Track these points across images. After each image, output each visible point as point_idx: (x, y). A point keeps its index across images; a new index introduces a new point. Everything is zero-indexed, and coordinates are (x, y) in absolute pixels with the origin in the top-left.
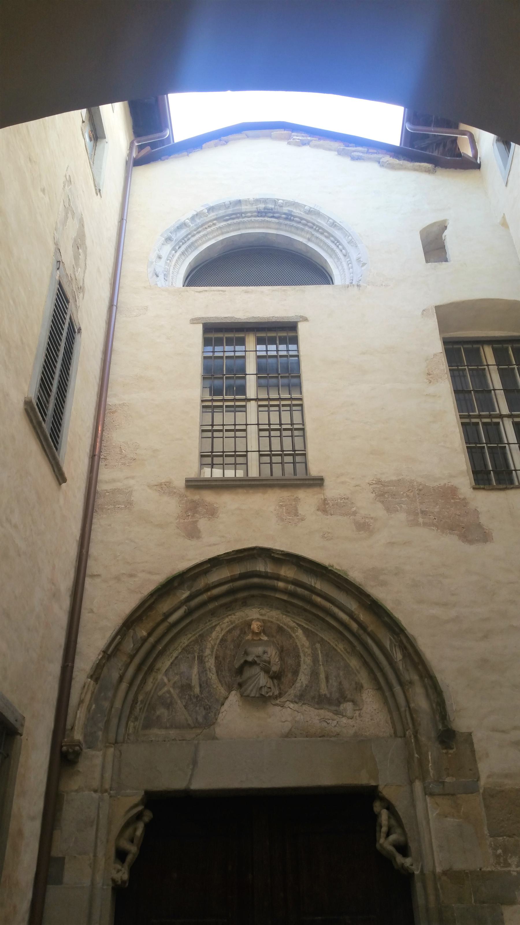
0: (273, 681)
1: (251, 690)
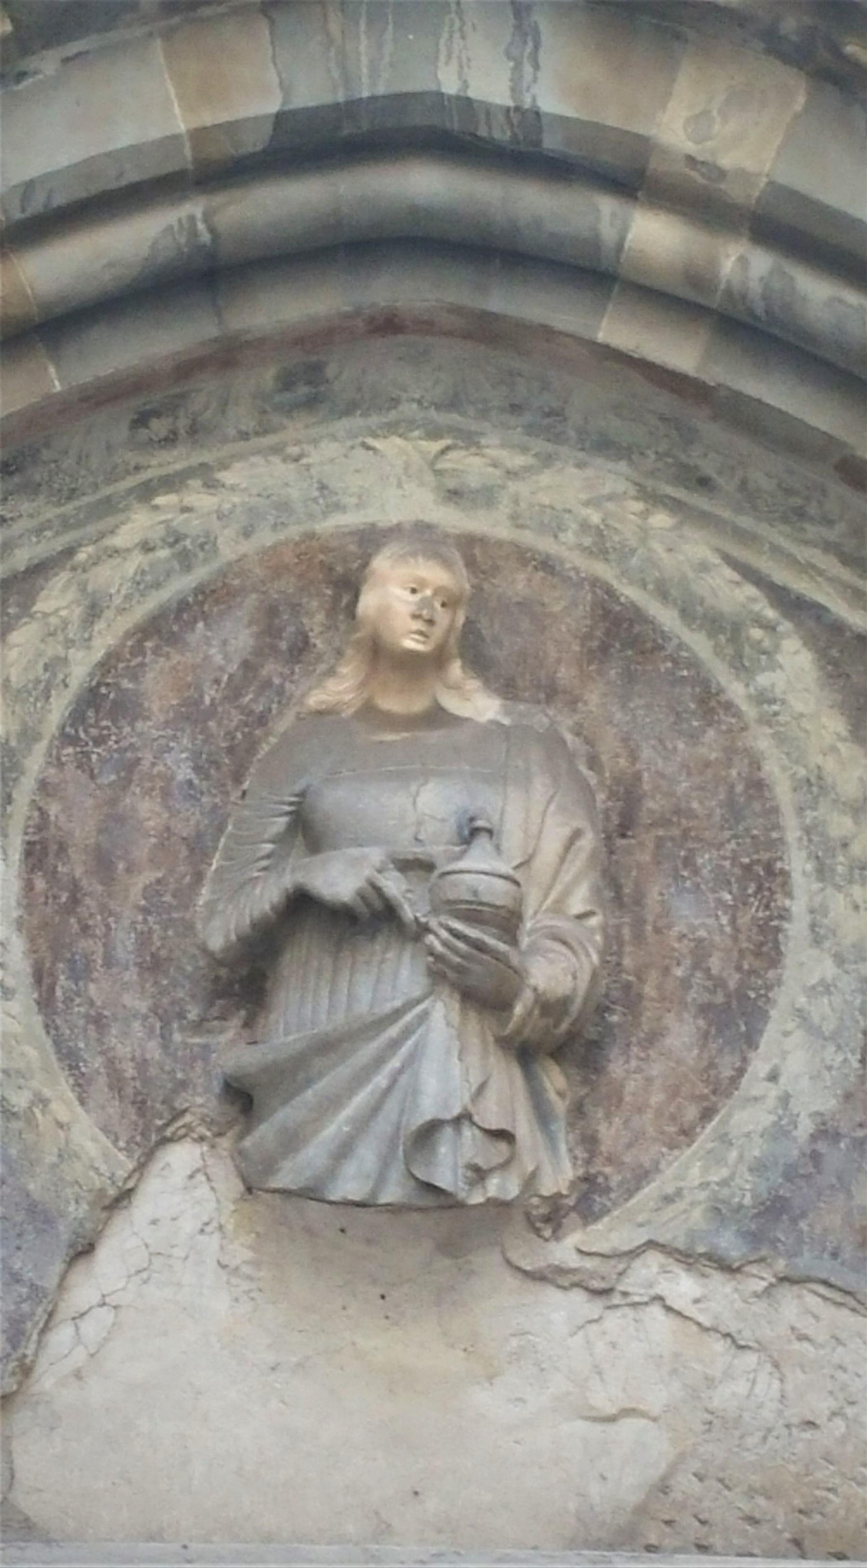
0: (530, 1076)
1: (340, 1141)
